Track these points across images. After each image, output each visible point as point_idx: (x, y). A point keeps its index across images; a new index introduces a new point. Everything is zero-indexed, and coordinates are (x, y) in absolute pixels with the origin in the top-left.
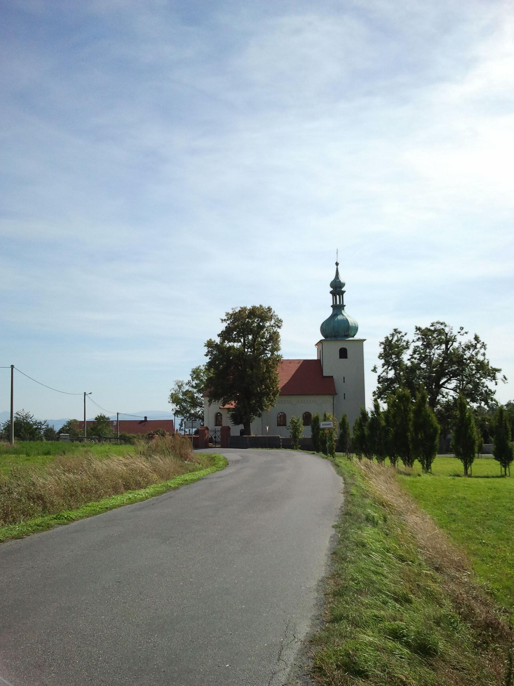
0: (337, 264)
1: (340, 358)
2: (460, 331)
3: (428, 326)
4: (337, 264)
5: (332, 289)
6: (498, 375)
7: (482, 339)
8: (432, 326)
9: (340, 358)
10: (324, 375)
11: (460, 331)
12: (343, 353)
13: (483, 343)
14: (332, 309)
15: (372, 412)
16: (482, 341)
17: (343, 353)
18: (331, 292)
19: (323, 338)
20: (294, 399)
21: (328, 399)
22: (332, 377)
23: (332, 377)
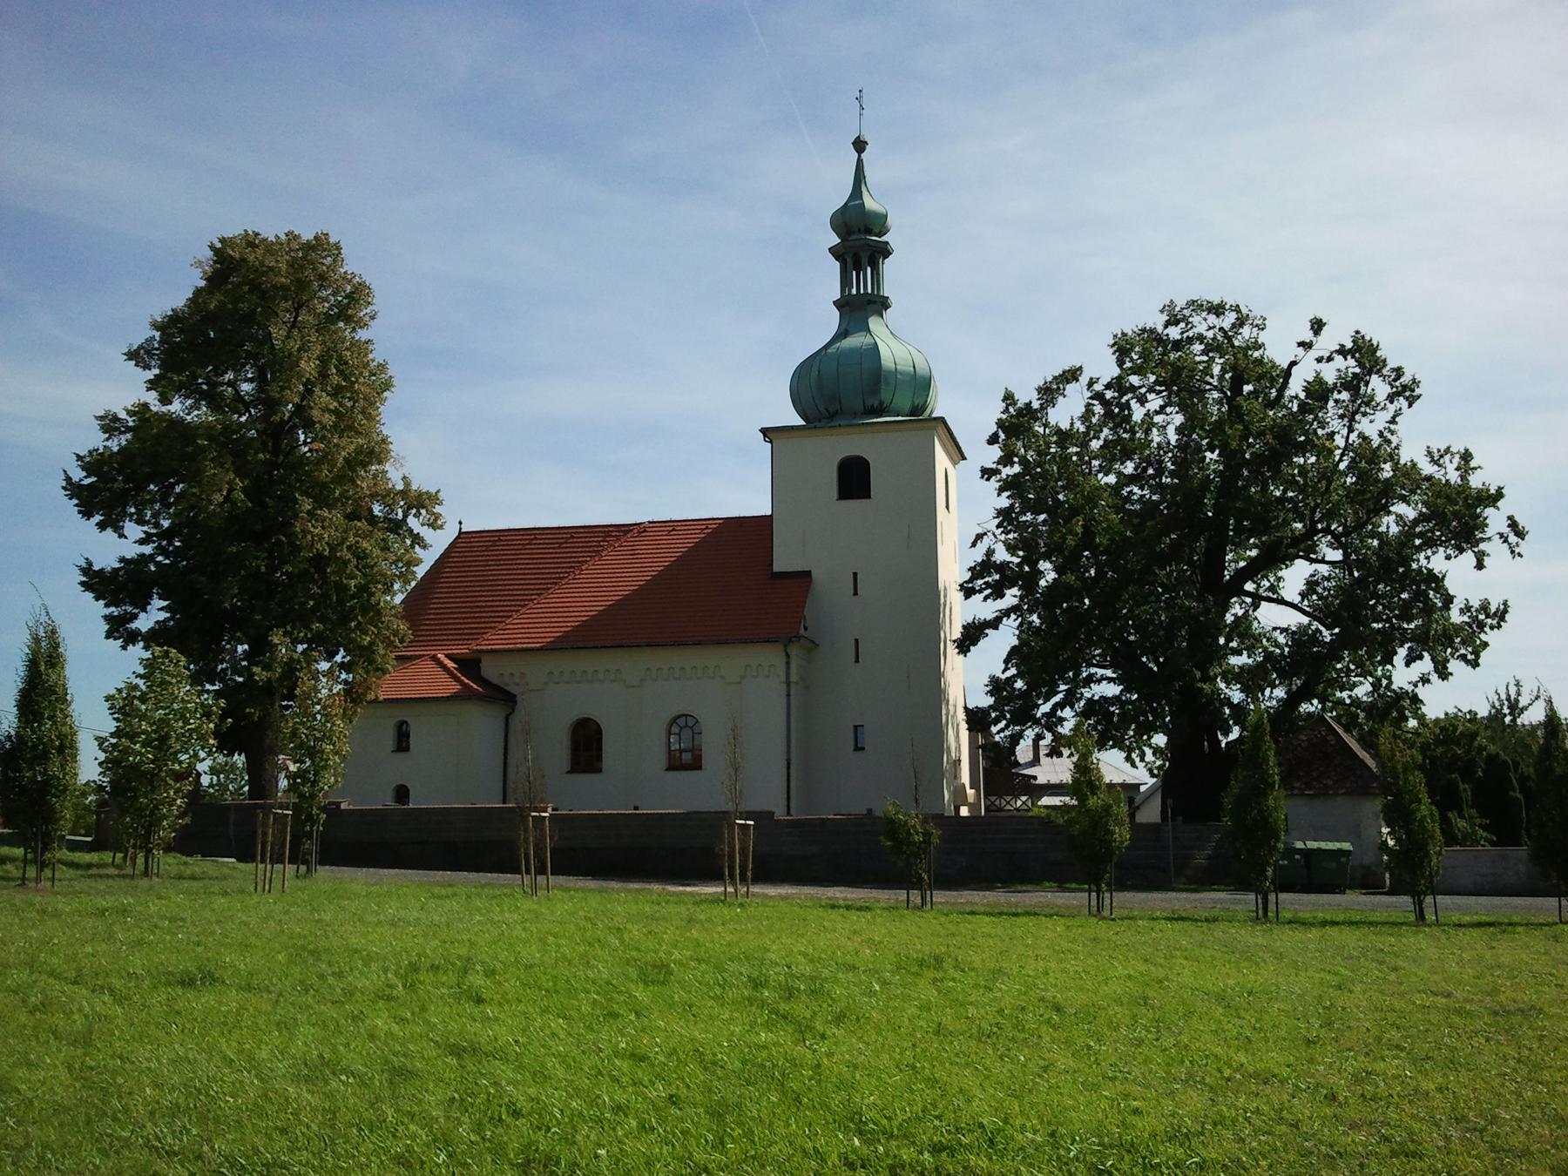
0: (860, 145)
1: (869, 497)
2: (1308, 336)
3: (1157, 321)
4: (860, 145)
5: (836, 240)
6: (1495, 520)
7: (1391, 354)
8: (1173, 321)
9: (869, 497)
10: (778, 566)
11: (1308, 336)
12: (854, 479)
13: (1399, 372)
14: (835, 314)
15: (107, 606)
16: (1392, 364)
17: (854, 479)
18: (834, 251)
19: (802, 422)
20: (634, 664)
21: (769, 658)
22: (809, 573)
23: (809, 573)
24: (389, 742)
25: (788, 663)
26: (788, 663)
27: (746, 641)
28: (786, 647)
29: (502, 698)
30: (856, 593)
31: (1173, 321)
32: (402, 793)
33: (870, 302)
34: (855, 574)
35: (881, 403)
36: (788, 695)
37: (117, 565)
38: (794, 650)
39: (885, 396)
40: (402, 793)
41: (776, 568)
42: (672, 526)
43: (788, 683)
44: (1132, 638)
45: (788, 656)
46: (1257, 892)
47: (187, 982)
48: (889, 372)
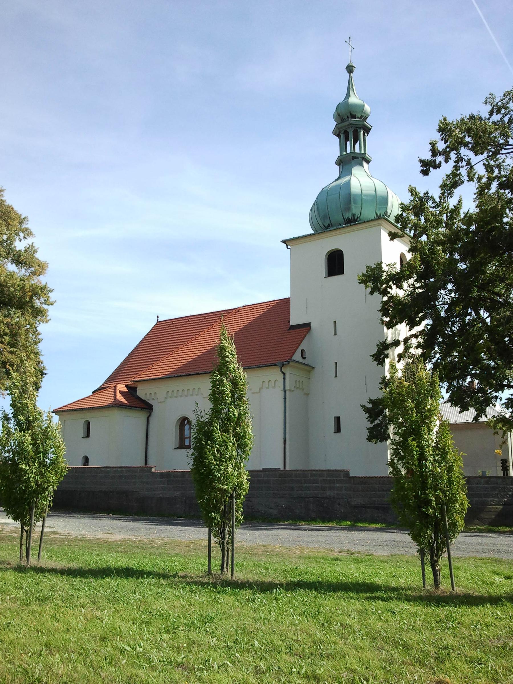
0: (350, 69)
4: (350, 69)
24: (81, 431)
25: (284, 379)
26: (284, 379)
27: (261, 367)
28: (281, 368)
29: (146, 407)
30: (335, 334)
31: (497, 109)
32: (86, 460)
33: (354, 158)
34: (335, 322)
35: (354, 215)
36: (285, 398)
37: (507, 401)
38: (287, 370)
39: (355, 210)
40: (86, 460)
41: (292, 323)
42: (252, 307)
43: (285, 391)
44: (456, 338)
45: (284, 374)
46: (209, 523)
47: (337, 559)
48: (356, 195)
